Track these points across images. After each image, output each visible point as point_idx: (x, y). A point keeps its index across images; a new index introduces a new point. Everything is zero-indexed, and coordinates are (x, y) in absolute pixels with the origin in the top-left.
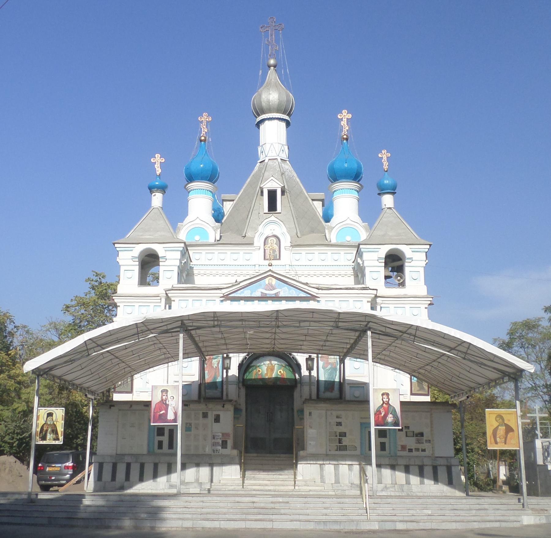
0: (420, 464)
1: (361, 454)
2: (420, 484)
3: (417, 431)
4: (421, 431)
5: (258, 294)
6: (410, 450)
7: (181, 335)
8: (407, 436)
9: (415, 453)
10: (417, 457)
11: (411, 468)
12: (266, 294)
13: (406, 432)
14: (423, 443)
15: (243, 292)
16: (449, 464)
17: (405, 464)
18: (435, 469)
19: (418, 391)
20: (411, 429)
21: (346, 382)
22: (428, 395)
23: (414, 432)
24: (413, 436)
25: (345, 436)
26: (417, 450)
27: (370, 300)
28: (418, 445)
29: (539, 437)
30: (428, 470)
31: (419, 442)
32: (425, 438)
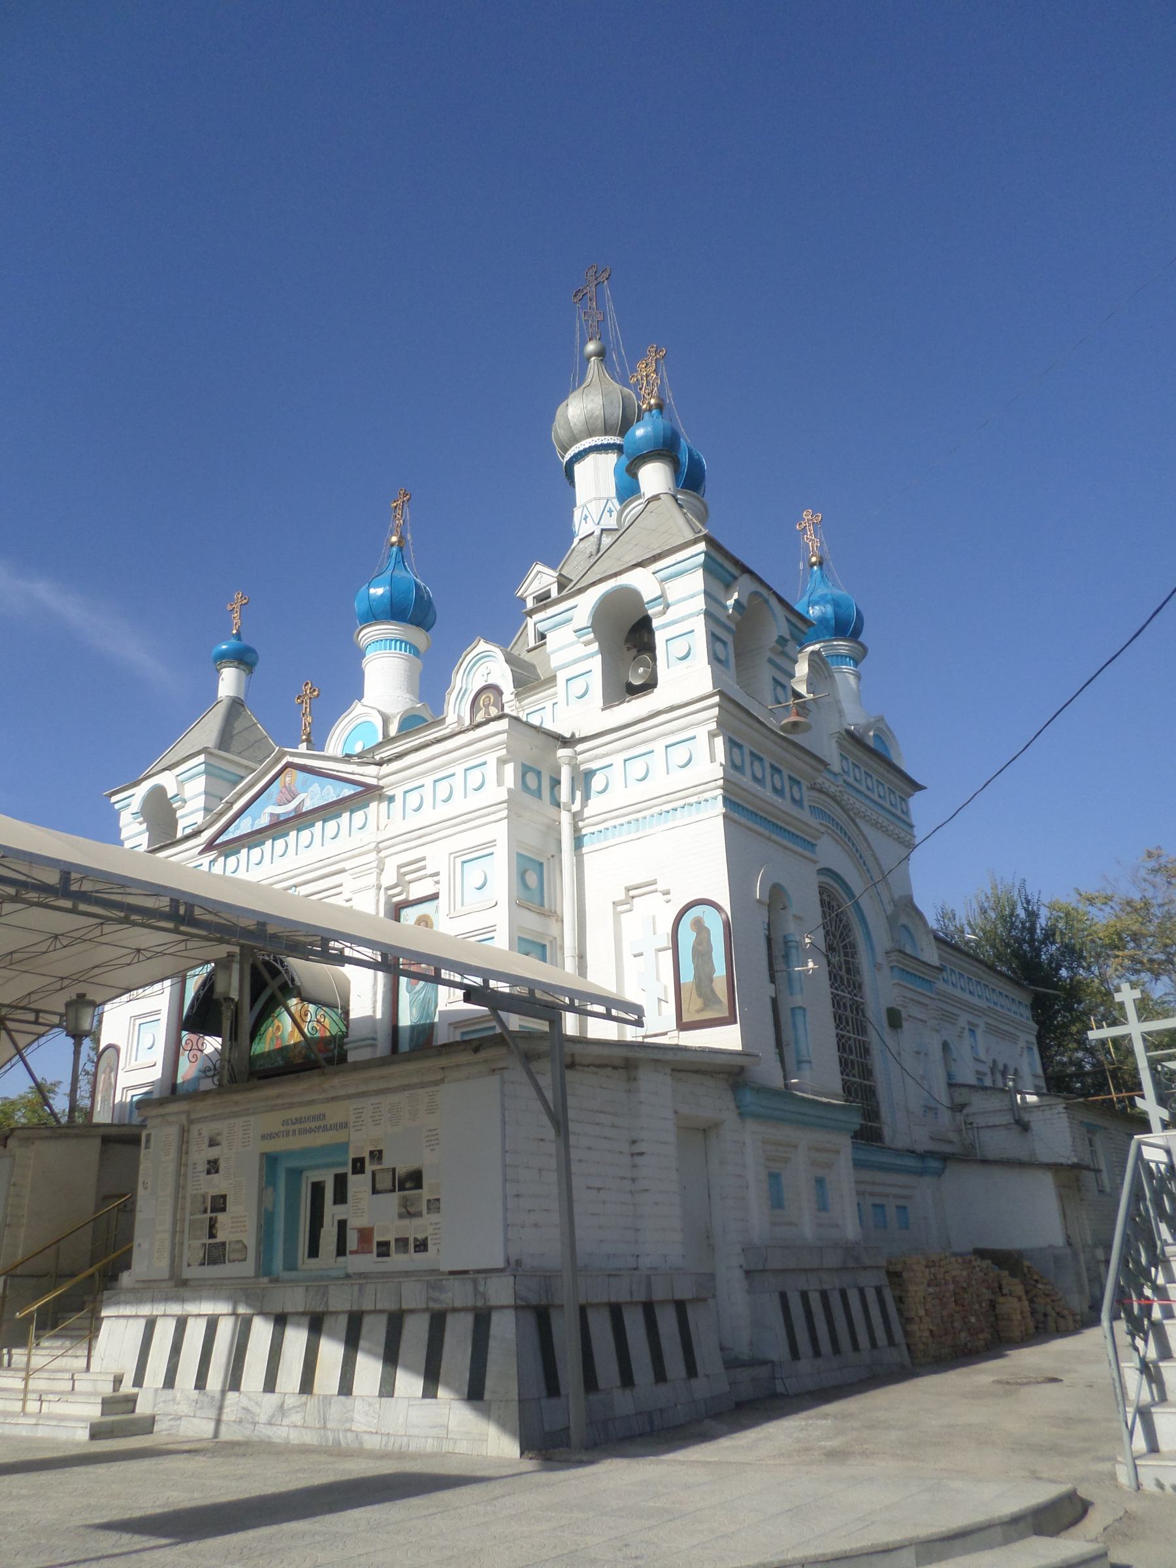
0: (391, 1306)
1: (171, 1279)
2: (381, 1395)
3: (402, 1169)
4: (414, 1166)
5: (264, 821)
6: (384, 1249)
7: (1094, 1035)
8: (375, 1191)
9: (398, 1261)
10: (407, 1274)
11: (328, 1323)
12: (278, 815)
13: (374, 1174)
14: (419, 1214)
15: (237, 828)
16: (480, 1304)
17: (349, 1309)
18: (396, 1322)
19: (699, 1011)
20: (387, 1162)
21: (354, 1034)
22: (731, 1020)
23: (394, 1170)
24: (393, 1191)
25: (371, 1230)
26: (402, 1243)
27: (713, 726)
28: (406, 1222)
29: (1155, 1124)
30: (375, 1330)
31: (408, 1212)
32: (426, 1193)
